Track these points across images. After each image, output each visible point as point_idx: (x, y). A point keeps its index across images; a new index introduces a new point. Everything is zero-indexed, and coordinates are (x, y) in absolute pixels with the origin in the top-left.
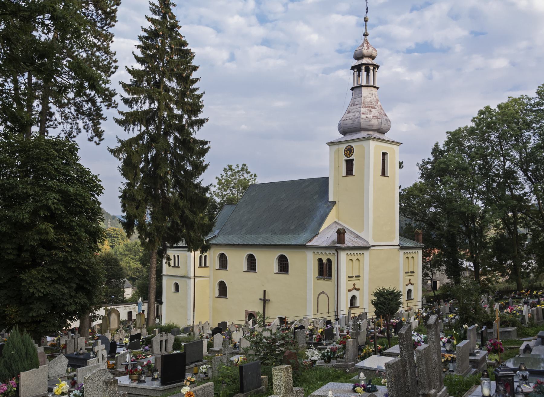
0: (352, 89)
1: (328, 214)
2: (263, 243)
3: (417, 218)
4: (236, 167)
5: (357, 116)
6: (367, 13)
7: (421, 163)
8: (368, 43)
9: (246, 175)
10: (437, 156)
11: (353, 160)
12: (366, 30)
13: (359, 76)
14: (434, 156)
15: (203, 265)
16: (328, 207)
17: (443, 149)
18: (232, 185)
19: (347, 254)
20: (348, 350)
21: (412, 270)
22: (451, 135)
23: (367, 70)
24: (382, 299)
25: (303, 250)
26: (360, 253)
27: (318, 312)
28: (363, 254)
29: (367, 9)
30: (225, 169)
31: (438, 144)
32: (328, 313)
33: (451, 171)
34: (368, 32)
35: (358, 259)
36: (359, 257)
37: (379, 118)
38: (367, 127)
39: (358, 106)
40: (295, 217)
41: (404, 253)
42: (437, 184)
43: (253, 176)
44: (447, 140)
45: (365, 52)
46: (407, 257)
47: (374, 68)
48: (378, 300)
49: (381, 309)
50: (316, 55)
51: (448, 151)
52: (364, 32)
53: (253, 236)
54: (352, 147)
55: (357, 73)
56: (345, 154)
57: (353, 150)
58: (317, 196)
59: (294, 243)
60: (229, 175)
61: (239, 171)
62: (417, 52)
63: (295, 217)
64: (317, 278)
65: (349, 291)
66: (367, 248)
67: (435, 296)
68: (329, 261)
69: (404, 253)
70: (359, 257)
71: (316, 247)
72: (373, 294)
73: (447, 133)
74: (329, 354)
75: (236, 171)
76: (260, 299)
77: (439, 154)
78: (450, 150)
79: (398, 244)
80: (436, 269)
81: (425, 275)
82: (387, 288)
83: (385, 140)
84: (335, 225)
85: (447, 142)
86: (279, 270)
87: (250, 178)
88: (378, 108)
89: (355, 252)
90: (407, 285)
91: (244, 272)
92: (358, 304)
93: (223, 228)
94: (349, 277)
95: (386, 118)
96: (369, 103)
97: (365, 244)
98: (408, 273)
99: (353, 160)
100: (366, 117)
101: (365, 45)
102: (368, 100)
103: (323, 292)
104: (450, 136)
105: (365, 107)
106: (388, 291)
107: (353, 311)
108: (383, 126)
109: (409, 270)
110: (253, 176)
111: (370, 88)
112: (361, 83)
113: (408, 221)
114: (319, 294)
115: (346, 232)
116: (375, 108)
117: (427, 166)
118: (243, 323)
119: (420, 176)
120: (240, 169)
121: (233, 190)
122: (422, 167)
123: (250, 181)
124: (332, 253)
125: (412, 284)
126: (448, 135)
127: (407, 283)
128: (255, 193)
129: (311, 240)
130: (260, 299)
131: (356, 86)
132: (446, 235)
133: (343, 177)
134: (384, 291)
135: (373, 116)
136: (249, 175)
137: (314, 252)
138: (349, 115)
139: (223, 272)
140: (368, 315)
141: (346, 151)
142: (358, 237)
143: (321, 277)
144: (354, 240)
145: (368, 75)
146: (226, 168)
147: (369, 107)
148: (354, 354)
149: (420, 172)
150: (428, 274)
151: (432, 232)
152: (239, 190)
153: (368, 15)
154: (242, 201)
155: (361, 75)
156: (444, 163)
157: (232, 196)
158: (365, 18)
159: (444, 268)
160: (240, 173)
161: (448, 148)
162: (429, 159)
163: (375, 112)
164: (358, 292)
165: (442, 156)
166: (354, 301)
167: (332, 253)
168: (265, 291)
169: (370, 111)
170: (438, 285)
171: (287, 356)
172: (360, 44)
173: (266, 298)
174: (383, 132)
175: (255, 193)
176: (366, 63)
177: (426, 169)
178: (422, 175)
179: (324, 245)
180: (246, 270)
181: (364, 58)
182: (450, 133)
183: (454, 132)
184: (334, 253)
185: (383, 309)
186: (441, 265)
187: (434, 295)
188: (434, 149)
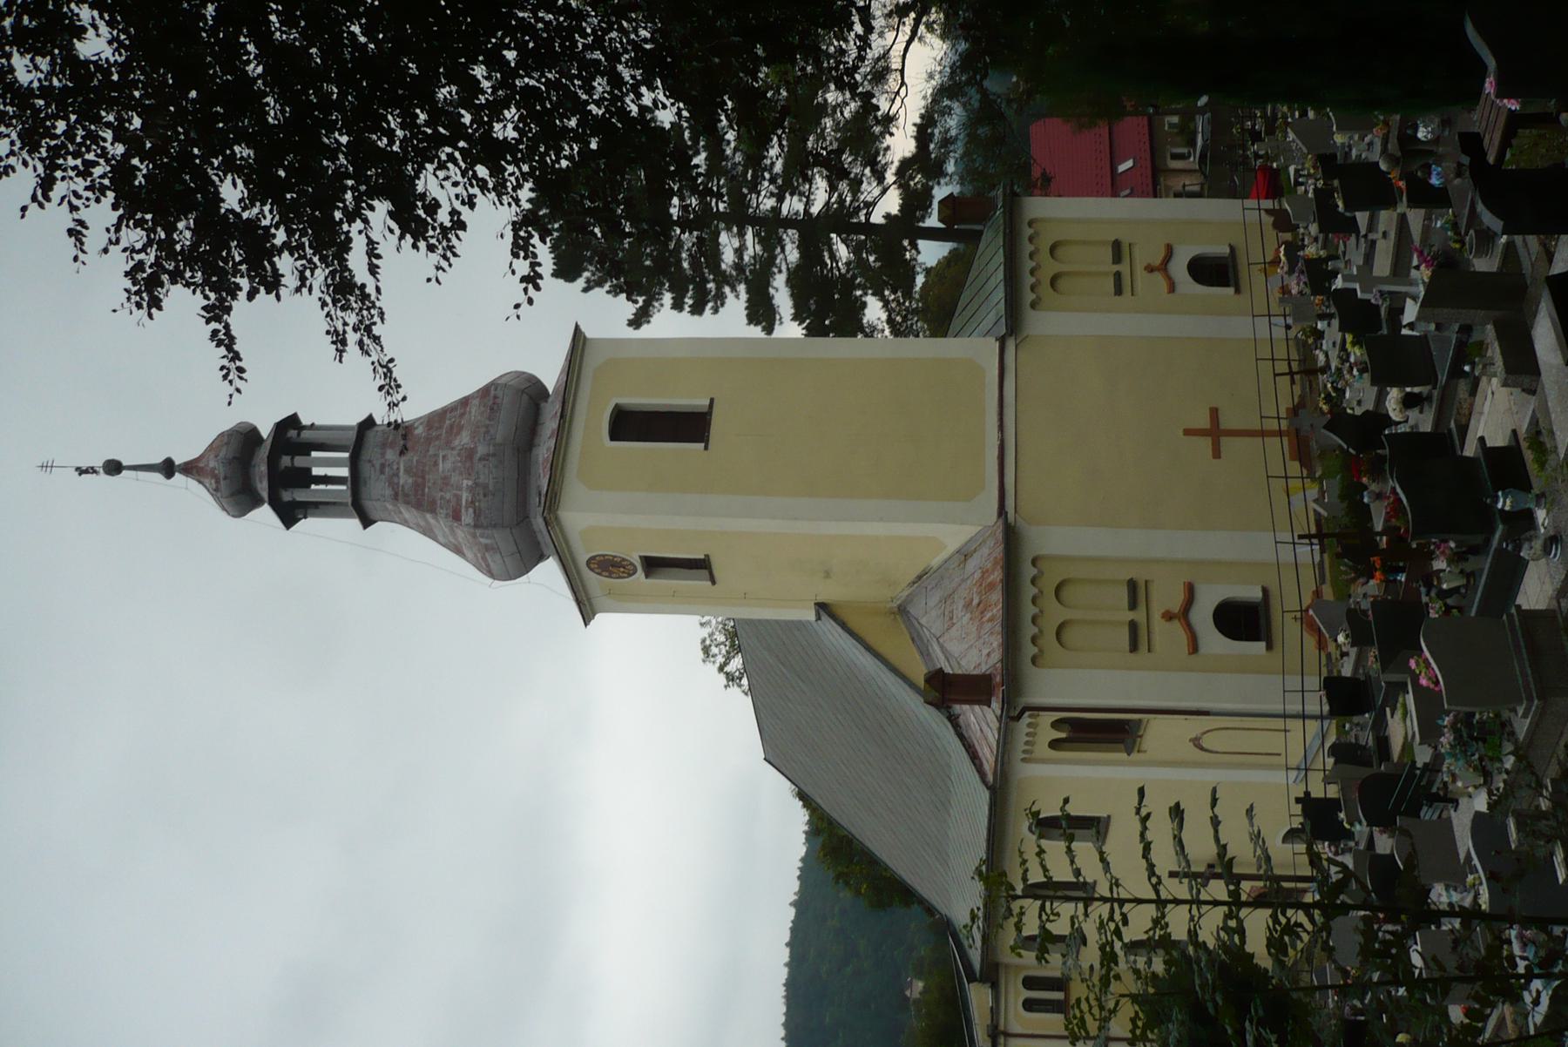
0: (367, 522)
15: (1058, 995)
34: (158, 459)
36: (1049, 587)
65: (1172, 288)
66: (1011, 538)
68: (1056, 725)
70: (1049, 587)
94: (1119, 291)
98: (1118, 276)
125: (1169, 252)
127: (1164, 285)
153: (98, 463)
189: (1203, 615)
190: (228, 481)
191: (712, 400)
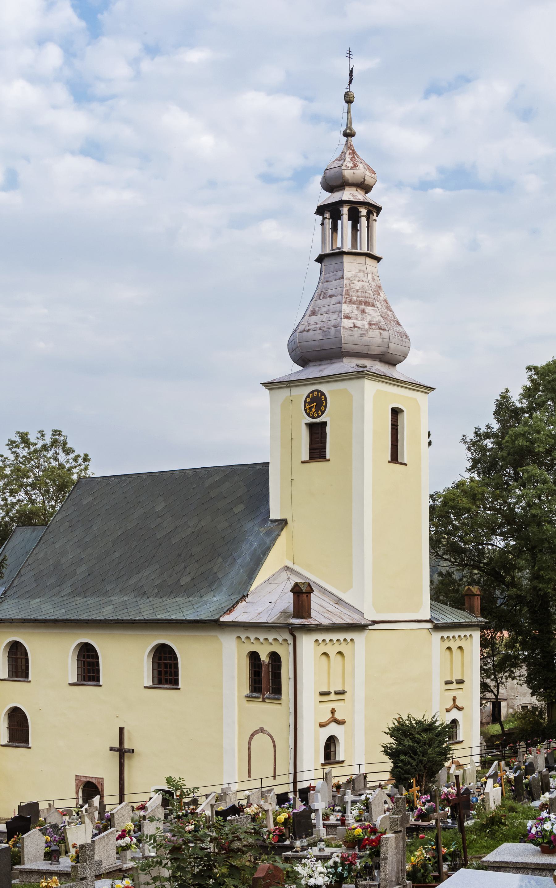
0: (320, 259)
1: (269, 549)
2: (116, 618)
3: (464, 560)
4: (39, 435)
5: (333, 323)
6: (350, 82)
7: (471, 436)
8: (354, 152)
9: (62, 458)
10: (508, 421)
11: (324, 424)
12: (349, 121)
13: (335, 229)
14: (499, 421)
16: (268, 533)
17: (519, 405)
18: (30, 480)
19: (317, 641)
20: (386, 859)
21: (459, 678)
22: (537, 373)
23: (354, 218)
24: (408, 743)
25: (213, 634)
26: (345, 640)
27: (250, 776)
28: (352, 640)
29: (351, 73)
30: (12, 443)
31: (509, 394)
32: (275, 777)
33: (537, 454)
34: (356, 127)
35: (340, 653)
36: (343, 648)
37: (384, 330)
38: (358, 349)
39: (334, 300)
40: (191, 555)
41: (442, 637)
42: (507, 483)
43: (80, 461)
44: (529, 384)
45: (348, 173)
46: (449, 648)
47: (369, 213)
48: (399, 744)
49: (405, 764)
50: (212, 184)
51: (530, 409)
52: (344, 128)
53: (91, 601)
54: (323, 394)
55: (329, 223)
56: (306, 410)
57: (326, 400)
58: (241, 507)
59: (190, 616)
60: (21, 455)
61: (45, 448)
62: (442, 188)
63: (191, 555)
64: (247, 697)
65: (322, 725)
66: (361, 627)
67: (504, 733)
69: (442, 637)
70: (343, 648)
71: (244, 626)
72: (388, 731)
73: (529, 369)
74: (340, 869)
75: (39, 446)
76: (112, 749)
77: (511, 417)
78: (534, 408)
79: (428, 618)
80: (507, 674)
81: (484, 687)
82: (419, 717)
83: (397, 380)
84: (285, 575)
85: (529, 389)
86: (156, 680)
87: (73, 464)
88: (379, 306)
89: (335, 636)
90: (448, 711)
91: (71, 684)
92: (340, 756)
93: (16, 583)
94: (322, 694)
95: (398, 329)
96: (359, 294)
97: (356, 619)
98: (451, 682)
99: (324, 424)
100: (355, 326)
101: (348, 157)
102: (358, 285)
103: (262, 730)
104: (535, 377)
105: (351, 302)
106: (420, 723)
107: (335, 771)
108: (393, 348)
109: (329, 686)
110: (80, 461)
111: (361, 260)
112: (339, 245)
113: (445, 566)
114: (253, 735)
115: (313, 591)
116: (373, 305)
117: (486, 442)
118: (71, 804)
119: (469, 464)
120: (48, 440)
121: (33, 492)
122: (473, 444)
123: (74, 471)
124: (281, 640)
125: (460, 709)
126: (530, 373)
127: (448, 707)
128: (91, 498)
129: (230, 610)
130: (112, 749)
131: (328, 251)
132: (529, 598)
133: (303, 462)
134: (411, 724)
135: (370, 324)
136: (72, 456)
137: (239, 637)
138: (314, 319)
139: (17, 686)
140: (368, 779)
141: (310, 403)
142: (339, 601)
143: (255, 695)
144: (331, 608)
145: (355, 229)
146: (14, 439)
147: (361, 302)
148: (398, 868)
149: (470, 455)
150: (490, 687)
151: (498, 593)
152: (48, 491)
153: (354, 89)
154: (59, 517)
155: (339, 227)
156: (523, 435)
157: (30, 506)
158: (346, 94)
159: (524, 671)
160: (48, 451)
161: (531, 402)
162: (488, 427)
163: (373, 314)
164: (342, 727)
165: (519, 421)
166: (332, 749)
167: (281, 640)
168: (121, 730)
169: (363, 311)
170: (504, 711)
171: (264, 878)
172: (338, 155)
173: (126, 746)
174: (393, 362)
175: (91, 498)
176: (352, 199)
177: (483, 449)
178: (475, 462)
179: (263, 619)
180: (75, 680)
181: (347, 189)
182: (535, 368)
183: (542, 367)
184: (285, 640)
185: (411, 765)
186: (516, 666)
187: (500, 731)
188: (500, 405)
189: (333, 729)
190: (353, 175)
191: (406, 465)
